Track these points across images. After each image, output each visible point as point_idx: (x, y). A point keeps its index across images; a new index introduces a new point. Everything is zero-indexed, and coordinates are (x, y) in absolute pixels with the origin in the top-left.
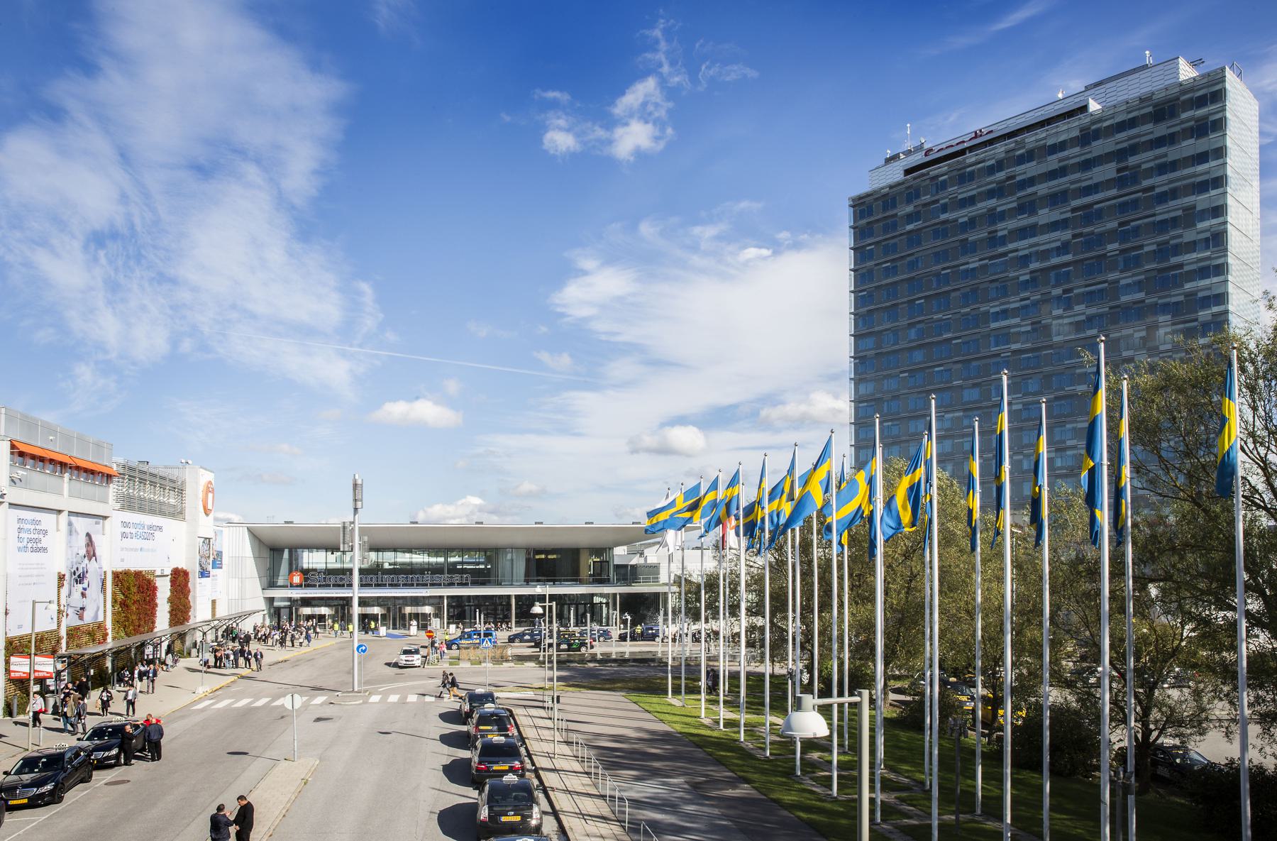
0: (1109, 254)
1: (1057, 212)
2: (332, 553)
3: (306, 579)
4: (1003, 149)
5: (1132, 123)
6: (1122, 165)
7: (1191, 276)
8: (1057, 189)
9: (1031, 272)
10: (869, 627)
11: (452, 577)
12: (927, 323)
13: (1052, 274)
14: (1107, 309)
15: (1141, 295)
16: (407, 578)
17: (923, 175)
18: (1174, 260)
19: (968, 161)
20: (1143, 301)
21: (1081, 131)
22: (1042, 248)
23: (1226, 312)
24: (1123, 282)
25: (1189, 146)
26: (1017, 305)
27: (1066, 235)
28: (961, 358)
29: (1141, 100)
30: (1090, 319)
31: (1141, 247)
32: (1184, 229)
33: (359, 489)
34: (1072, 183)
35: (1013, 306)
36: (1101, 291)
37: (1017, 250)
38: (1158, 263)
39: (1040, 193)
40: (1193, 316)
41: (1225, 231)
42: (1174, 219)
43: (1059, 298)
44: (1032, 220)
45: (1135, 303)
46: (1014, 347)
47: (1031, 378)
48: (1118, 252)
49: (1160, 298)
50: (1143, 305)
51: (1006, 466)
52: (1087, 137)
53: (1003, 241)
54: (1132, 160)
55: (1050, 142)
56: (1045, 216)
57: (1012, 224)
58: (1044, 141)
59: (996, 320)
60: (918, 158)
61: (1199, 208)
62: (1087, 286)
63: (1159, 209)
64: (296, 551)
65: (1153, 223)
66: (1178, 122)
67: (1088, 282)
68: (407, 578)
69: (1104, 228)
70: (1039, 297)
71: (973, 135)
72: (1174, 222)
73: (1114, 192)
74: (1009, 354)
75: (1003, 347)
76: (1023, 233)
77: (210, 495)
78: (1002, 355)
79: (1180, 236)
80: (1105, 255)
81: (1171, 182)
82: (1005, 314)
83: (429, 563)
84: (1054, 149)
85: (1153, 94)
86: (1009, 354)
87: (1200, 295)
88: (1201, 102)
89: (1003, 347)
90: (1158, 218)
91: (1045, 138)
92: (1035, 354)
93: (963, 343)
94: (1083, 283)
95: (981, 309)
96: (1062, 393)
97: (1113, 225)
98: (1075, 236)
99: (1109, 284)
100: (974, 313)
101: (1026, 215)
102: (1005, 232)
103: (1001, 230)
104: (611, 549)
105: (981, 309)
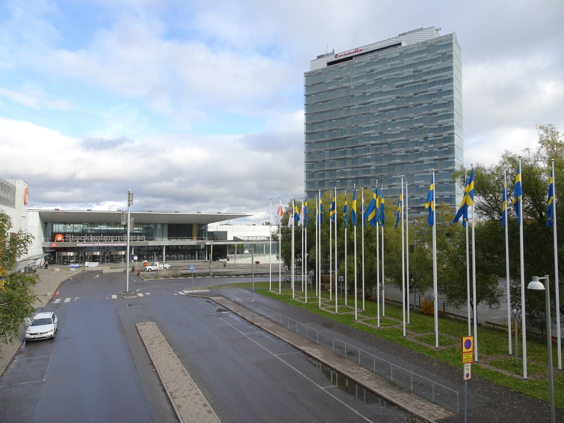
0: (410, 106)
2: (69, 225)
3: (65, 238)
4: (369, 58)
6: (415, 70)
7: (440, 118)
8: (390, 77)
9: (380, 112)
10: (296, 257)
11: (136, 237)
13: (387, 113)
15: (421, 124)
16: (115, 237)
17: (336, 66)
19: (355, 62)
21: (400, 54)
22: (384, 102)
23: (453, 133)
24: (415, 118)
25: (439, 65)
26: (374, 125)
27: (393, 97)
28: (350, 146)
29: (423, 43)
30: (402, 132)
31: (422, 104)
32: (438, 98)
33: (131, 196)
35: (372, 125)
36: (406, 121)
38: (428, 111)
40: (441, 134)
41: (453, 101)
42: (434, 94)
48: (413, 106)
49: (429, 126)
50: (422, 128)
52: (402, 55)
55: (388, 57)
56: (385, 88)
57: (372, 90)
59: (365, 131)
60: (333, 59)
61: (443, 90)
63: (429, 89)
64: (250, 256)
65: (426, 95)
68: (115, 237)
71: (355, 50)
72: (434, 95)
73: (412, 81)
74: (370, 145)
77: (27, 195)
78: (367, 146)
81: (433, 78)
82: (368, 128)
83: (108, 230)
84: (390, 59)
85: (427, 41)
86: (370, 145)
87: (444, 126)
88: (444, 46)
90: (428, 93)
91: (386, 55)
92: (380, 146)
93: (351, 139)
98: (397, 98)
100: (357, 127)
103: (368, 93)
104: (207, 224)
105: (359, 126)
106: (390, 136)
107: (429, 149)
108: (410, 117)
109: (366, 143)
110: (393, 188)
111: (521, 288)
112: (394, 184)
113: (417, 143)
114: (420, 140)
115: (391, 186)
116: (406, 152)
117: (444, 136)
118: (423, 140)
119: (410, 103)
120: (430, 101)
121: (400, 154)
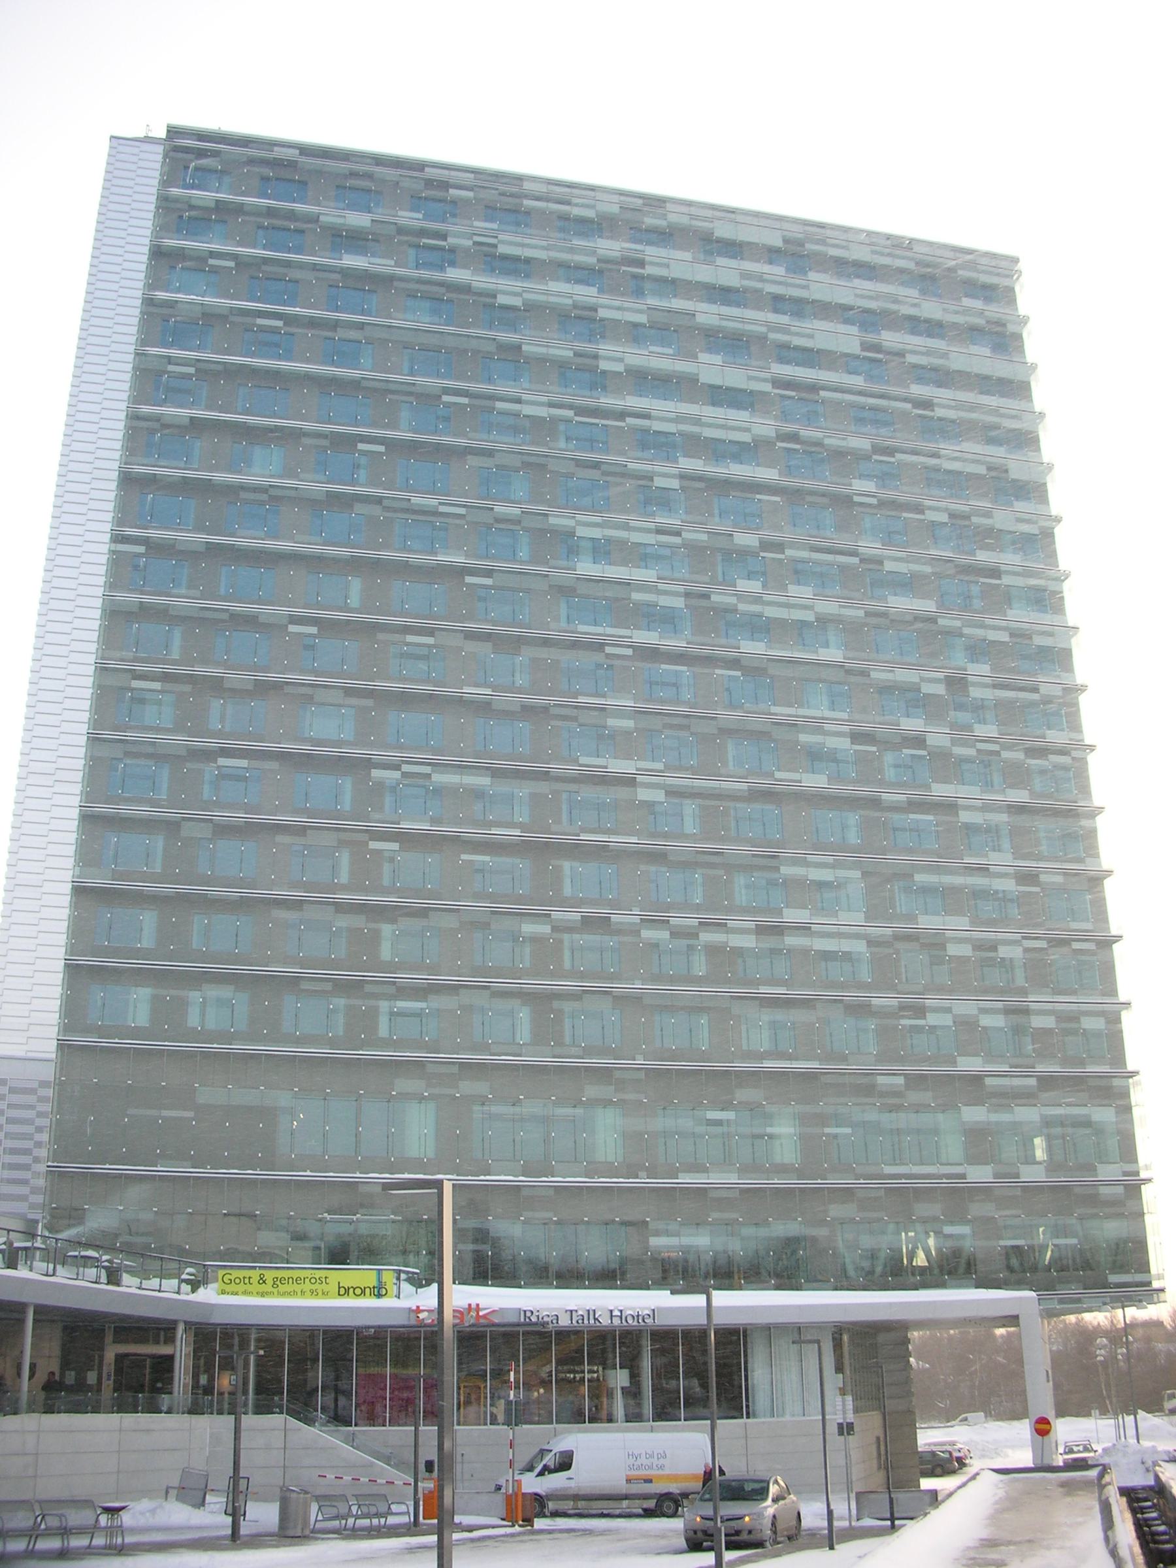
14: (861, 613)
15: (928, 606)
27: (764, 426)
30: (823, 621)
38: (467, 556)
39: (701, 319)
44: (683, 366)
48: (874, 501)
53: (601, 381)
54: (890, 338)
70: (704, 537)
73: (858, 381)
74: (629, 652)
75: (610, 631)
76: (643, 380)
78: (608, 650)
79: (988, 514)
86: (629, 652)
89: (610, 631)
95: (552, 520)
96: (763, 783)
99: (862, 561)
101: (671, 351)
102: (619, 368)
106: (759, 627)
107: (980, 746)
108: (861, 550)
109: (599, 630)
110: (791, 941)
111: (1006, 1317)
112: (792, 916)
113: (913, 699)
114: (927, 689)
115: (778, 930)
116: (856, 737)
117: (1044, 689)
118: (940, 690)
119: (859, 485)
120: (960, 507)
121: (818, 739)
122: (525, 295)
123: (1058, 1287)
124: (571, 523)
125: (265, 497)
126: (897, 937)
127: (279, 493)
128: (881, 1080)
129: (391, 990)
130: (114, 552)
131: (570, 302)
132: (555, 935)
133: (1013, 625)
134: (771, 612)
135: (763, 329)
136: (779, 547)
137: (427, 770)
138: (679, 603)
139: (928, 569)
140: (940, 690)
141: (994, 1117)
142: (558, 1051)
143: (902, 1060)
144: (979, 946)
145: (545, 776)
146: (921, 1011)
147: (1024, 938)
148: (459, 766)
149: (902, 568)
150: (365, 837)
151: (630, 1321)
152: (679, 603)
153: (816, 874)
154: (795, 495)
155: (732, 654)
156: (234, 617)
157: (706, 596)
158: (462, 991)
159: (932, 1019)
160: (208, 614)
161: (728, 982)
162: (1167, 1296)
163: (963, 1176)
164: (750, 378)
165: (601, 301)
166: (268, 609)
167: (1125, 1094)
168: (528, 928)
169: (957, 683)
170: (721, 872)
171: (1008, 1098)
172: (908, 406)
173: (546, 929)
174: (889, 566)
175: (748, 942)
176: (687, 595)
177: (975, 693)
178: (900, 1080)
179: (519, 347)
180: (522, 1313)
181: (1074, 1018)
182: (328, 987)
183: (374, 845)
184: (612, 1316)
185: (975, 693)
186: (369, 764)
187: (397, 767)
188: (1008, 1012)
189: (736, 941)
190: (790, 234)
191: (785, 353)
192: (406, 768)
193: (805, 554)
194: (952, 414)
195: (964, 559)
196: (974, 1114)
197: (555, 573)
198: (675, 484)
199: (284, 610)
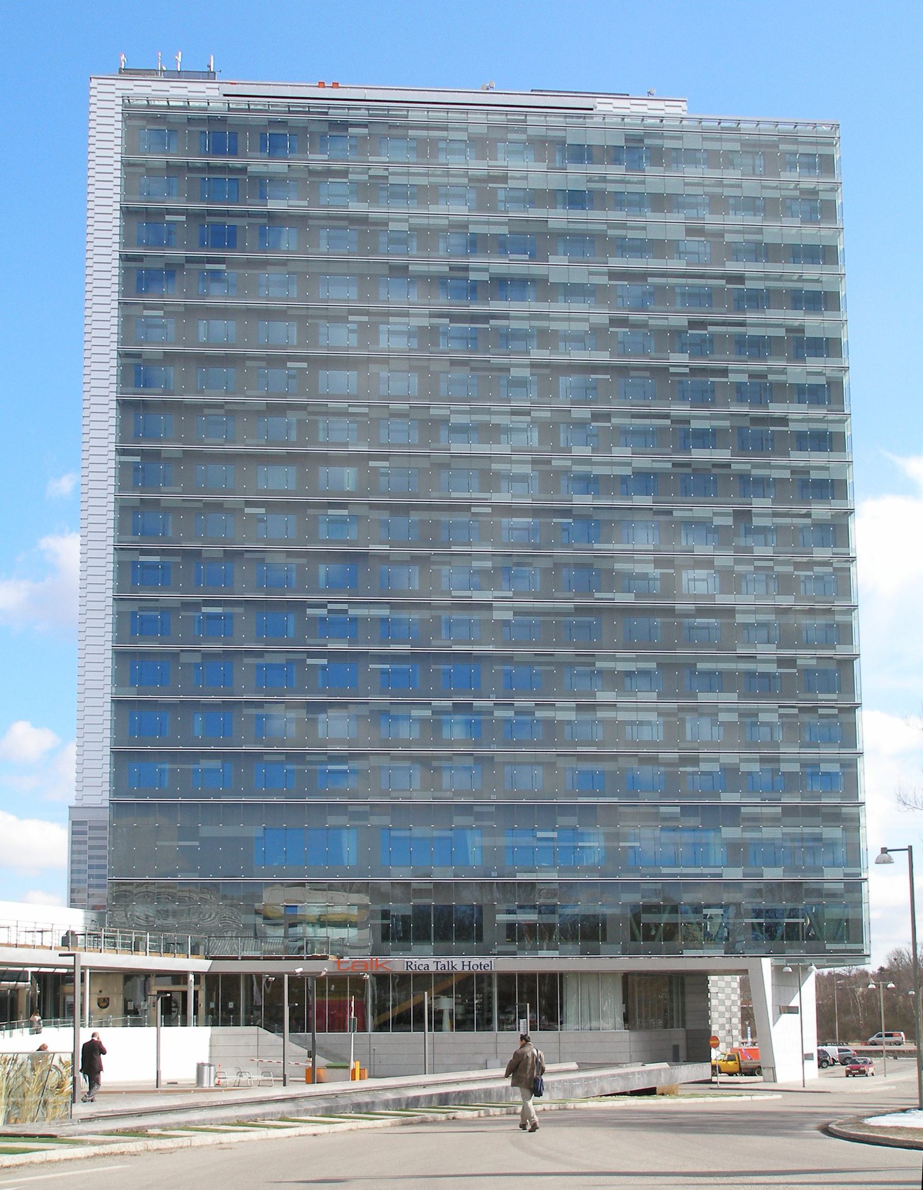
0: (672, 370)
1: (583, 268)
5: (725, 160)
12: (310, 413)
18: (776, 409)
20: (728, 466)
32: (788, 360)
34: (612, 226)
37: (506, 317)
38: (751, 407)
39: (552, 224)
43: (581, 424)
44: (537, 269)
45: (715, 465)
46: (502, 498)
47: (449, 563)
48: (687, 370)
51: (204, 699)
58: (562, 134)
62: (634, 416)
63: (751, 316)
66: (774, 184)
67: (635, 410)
69: (665, 323)
70: (548, 414)
74: (489, 510)
80: (666, 369)
86: (489, 510)
94: (627, 408)
95: (432, 411)
97: (679, 320)
102: (485, 277)
110: (600, 714)
112: (604, 696)
115: (593, 707)
122: (412, 221)
123: (787, 951)
124: (447, 412)
125: (222, 412)
126: (681, 709)
127: (235, 407)
128: (662, 809)
129: (324, 758)
130: (120, 463)
131: (446, 222)
132: (435, 717)
133: (794, 464)
134: (597, 471)
135: (604, 227)
136: (607, 417)
137: (345, 607)
138: (527, 469)
139: (726, 423)
140: (729, 521)
141: (748, 835)
142: (437, 794)
143: (679, 796)
144: (743, 714)
145: (428, 606)
146: (695, 761)
147: (780, 707)
148: (367, 603)
149: (705, 425)
150: (304, 656)
151: (475, 968)
152: (527, 469)
153: (622, 667)
154: (622, 371)
155: (565, 505)
156: (208, 505)
157: (549, 462)
158: (371, 757)
159: (704, 767)
160: (187, 505)
161: (555, 745)
162: (872, 959)
163: (721, 875)
164: (591, 273)
165: (472, 219)
166: (230, 498)
167: (856, 819)
168: (416, 713)
169: (743, 516)
170: (553, 668)
171: (755, 821)
172: (723, 282)
173: (428, 713)
174: (695, 424)
175: (571, 716)
176: (534, 462)
177: (757, 522)
178: (678, 810)
179: (406, 267)
180: (406, 963)
181: (816, 764)
182: (283, 758)
183: (310, 661)
184: (463, 965)
185: (757, 522)
186: (304, 605)
187: (324, 606)
188: (762, 760)
189: (561, 716)
190: (632, 132)
191: (624, 247)
192: (330, 606)
193: (627, 421)
194: (760, 285)
195: (759, 412)
196: (730, 833)
197: (435, 453)
198: (526, 373)
199: (240, 498)
